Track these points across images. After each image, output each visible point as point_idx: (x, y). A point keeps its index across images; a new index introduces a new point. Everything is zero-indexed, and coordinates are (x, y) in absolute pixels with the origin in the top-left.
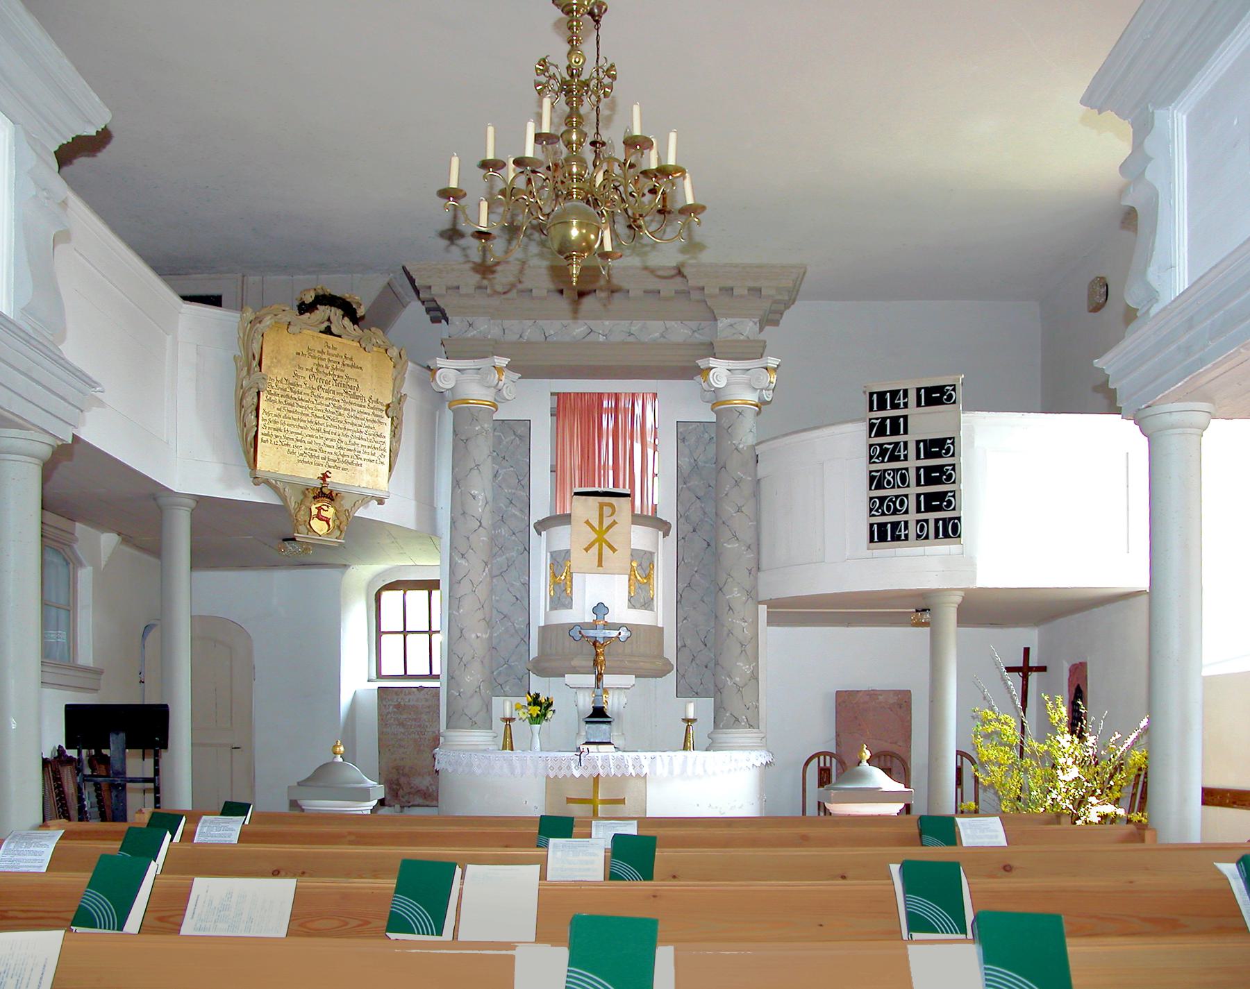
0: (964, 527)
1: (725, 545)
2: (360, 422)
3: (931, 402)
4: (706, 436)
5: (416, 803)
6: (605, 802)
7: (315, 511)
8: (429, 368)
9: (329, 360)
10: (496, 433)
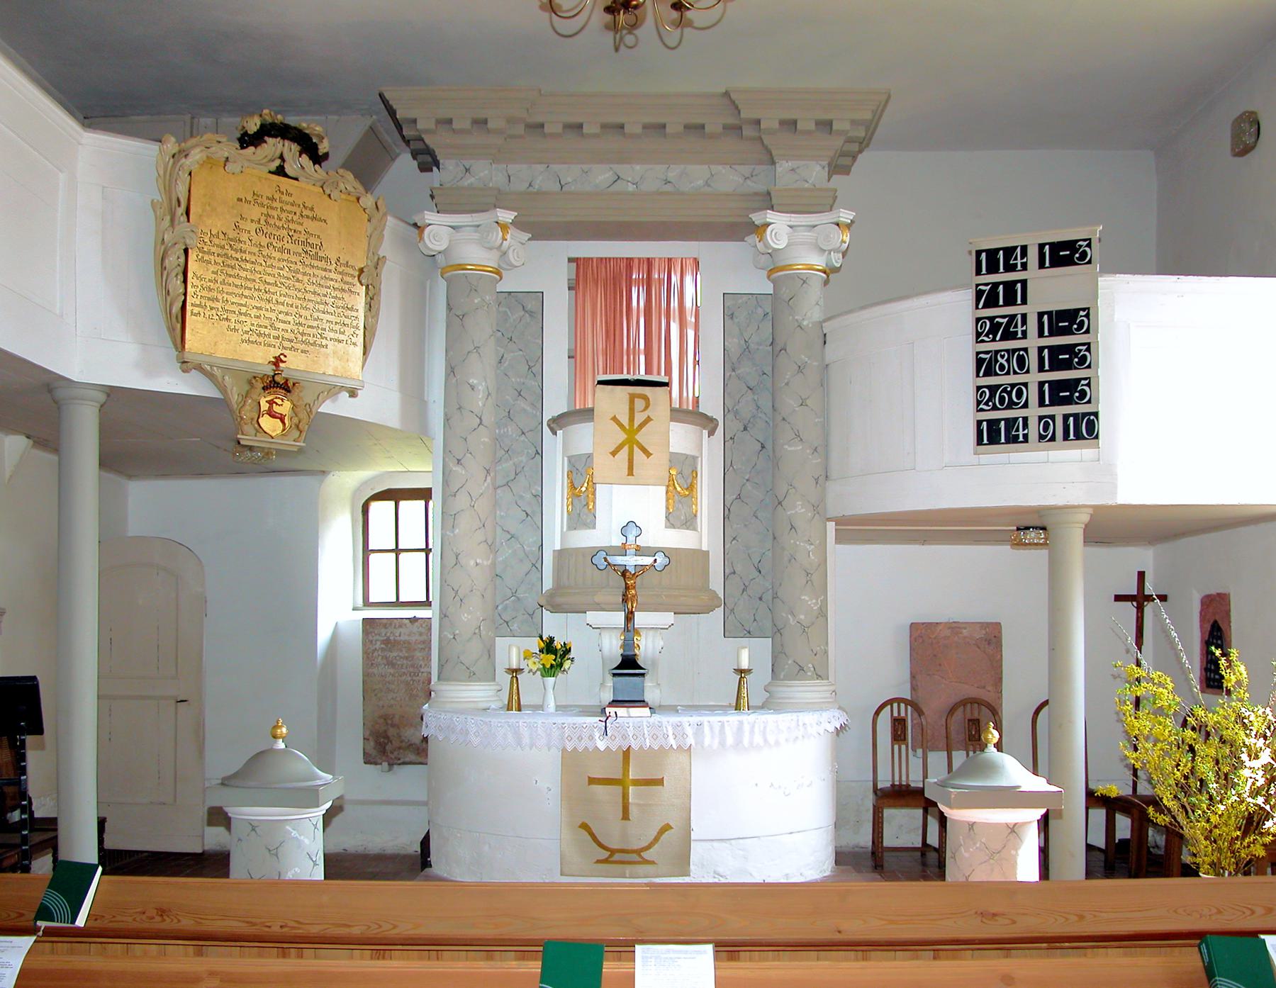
0: (1103, 426)
1: (786, 447)
2: (324, 291)
3: (1057, 262)
4: (760, 311)
5: (407, 760)
6: (637, 783)
7: (265, 406)
8: (415, 225)
9: (282, 209)
10: (501, 309)
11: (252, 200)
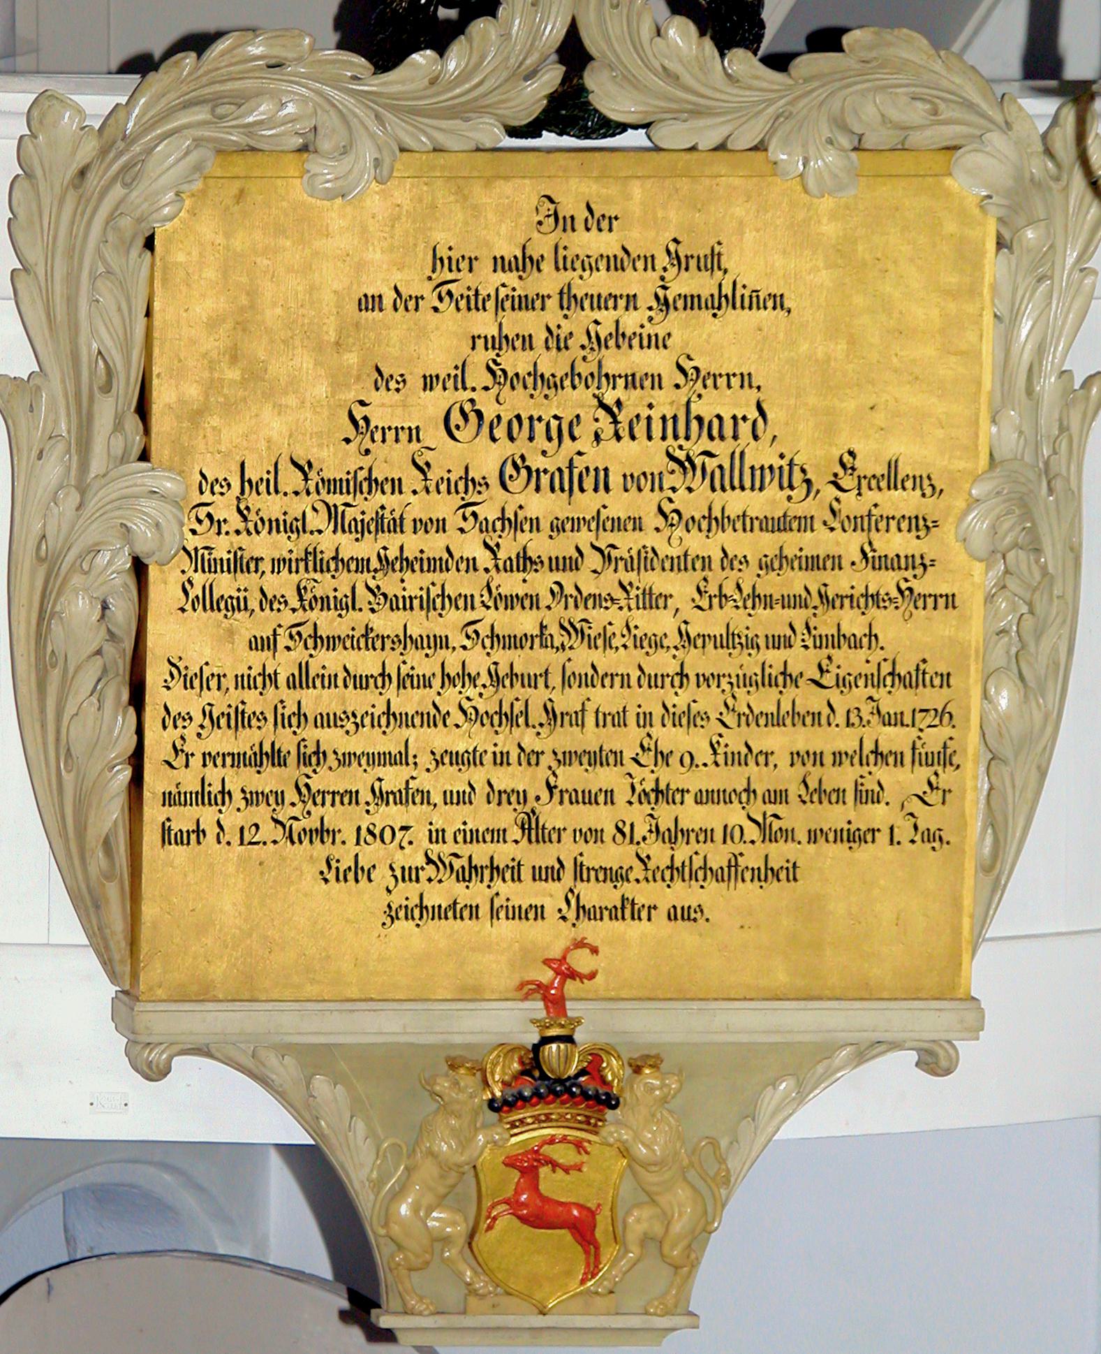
11: (426, 289)
